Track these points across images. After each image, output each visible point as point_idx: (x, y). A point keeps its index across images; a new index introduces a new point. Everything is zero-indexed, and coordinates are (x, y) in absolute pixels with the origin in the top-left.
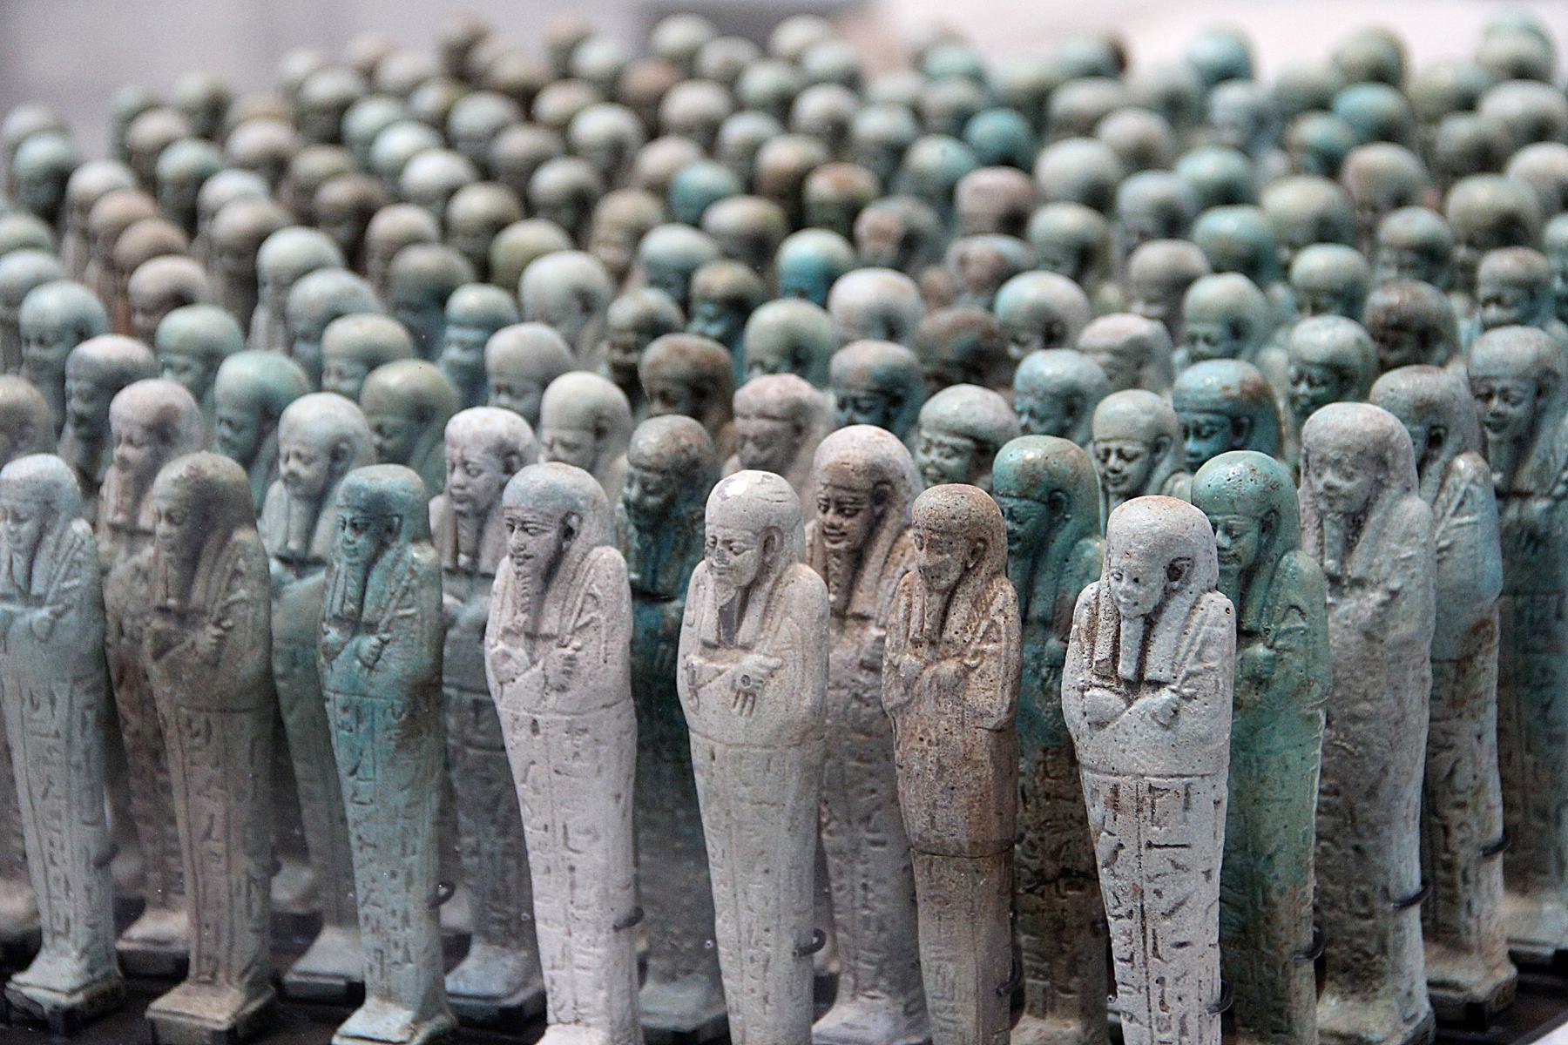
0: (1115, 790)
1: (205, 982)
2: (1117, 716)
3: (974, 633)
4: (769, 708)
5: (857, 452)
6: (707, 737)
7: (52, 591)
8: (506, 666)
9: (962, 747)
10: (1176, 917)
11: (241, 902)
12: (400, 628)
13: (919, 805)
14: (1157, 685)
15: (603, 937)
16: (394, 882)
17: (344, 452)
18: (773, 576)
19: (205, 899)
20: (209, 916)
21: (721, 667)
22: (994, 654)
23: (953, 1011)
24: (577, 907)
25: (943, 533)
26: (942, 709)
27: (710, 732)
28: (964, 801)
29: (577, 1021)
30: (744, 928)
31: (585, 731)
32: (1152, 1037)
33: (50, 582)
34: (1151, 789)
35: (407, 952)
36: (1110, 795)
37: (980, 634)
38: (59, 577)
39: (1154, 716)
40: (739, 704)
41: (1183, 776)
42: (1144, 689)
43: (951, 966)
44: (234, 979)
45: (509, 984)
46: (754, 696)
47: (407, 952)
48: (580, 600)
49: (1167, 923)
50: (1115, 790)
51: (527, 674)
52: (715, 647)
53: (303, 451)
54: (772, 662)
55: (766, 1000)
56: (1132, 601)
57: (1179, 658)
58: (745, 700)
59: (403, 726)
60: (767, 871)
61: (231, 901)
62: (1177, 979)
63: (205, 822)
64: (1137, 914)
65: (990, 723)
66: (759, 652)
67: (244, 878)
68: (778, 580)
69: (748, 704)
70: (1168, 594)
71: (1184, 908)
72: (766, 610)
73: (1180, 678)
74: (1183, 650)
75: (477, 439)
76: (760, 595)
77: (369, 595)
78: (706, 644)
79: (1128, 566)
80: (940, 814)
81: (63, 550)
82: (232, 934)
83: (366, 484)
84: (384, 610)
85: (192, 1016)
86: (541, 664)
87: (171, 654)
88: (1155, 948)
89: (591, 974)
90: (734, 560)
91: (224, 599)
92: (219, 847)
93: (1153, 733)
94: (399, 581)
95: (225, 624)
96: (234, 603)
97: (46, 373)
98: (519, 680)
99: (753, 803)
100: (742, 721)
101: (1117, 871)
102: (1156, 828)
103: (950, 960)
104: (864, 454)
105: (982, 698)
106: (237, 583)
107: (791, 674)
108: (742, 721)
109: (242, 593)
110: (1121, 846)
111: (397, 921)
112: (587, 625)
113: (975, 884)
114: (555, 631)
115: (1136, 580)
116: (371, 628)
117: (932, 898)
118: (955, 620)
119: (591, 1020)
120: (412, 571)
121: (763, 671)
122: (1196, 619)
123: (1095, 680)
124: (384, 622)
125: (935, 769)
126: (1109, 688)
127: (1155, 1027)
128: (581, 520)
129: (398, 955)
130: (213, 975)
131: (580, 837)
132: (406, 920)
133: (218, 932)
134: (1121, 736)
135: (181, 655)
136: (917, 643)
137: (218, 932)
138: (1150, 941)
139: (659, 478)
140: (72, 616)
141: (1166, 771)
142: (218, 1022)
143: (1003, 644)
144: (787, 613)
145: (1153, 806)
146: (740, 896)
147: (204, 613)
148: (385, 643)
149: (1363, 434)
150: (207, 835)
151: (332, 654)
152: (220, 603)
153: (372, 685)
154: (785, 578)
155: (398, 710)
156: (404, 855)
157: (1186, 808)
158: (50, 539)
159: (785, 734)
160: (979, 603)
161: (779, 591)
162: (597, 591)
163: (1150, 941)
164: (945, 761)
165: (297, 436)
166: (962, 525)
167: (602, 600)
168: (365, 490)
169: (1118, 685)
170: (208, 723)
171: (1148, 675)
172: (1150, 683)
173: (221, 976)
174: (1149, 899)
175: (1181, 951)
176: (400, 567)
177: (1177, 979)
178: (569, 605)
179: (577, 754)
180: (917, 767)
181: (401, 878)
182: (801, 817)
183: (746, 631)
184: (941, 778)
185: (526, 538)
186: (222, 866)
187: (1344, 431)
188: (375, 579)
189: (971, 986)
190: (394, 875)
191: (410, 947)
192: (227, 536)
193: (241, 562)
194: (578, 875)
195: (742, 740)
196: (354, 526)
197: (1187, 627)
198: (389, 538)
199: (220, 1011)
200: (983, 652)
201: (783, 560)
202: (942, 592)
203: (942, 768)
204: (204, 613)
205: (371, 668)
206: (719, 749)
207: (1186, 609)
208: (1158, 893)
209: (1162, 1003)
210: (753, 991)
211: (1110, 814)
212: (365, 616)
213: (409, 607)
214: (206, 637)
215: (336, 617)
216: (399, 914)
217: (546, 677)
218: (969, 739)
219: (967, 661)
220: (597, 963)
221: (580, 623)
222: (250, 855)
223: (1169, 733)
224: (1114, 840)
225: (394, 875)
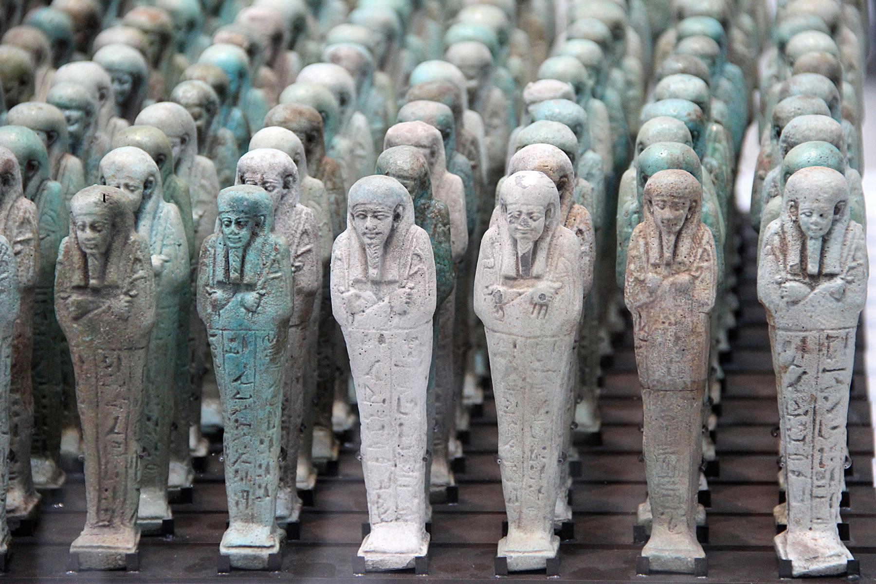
0: (804, 340)
1: (104, 526)
2: (806, 296)
3: (695, 256)
4: (557, 312)
5: (550, 159)
6: (510, 334)
8: (358, 303)
9: (691, 324)
10: (834, 412)
11: (131, 471)
12: (272, 286)
13: (660, 362)
14: (832, 276)
15: (418, 465)
16: (263, 446)
17: (151, 182)
18: (550, 233)
19: (106, 472)
20: (107, 483)
21: (521, 291)
22: (708, 268)
23: (674, 483)
24: (402, 449)
25: (680, 198)
26: (678, 303)
27: (514, 331)
28: (690, 357)
29: (397, 519)
30: (527, 450)
31: (416, 338)
32: (812, 483)
34: (828, 337)
35: (266, 490)
36: (800, 343)
37: (699, 257)
39: (832, 294)
40: (536, 312)
41: (845, 328)
42: (822, 279)
43: (673, 457)
44: (126, 522)
45: (287, 508)
46: (547, 306)
47: (266, 490)
48: (410, 258)
49: (830, 415)
50: (804, 340)
51: (375, 306)
52: (515, 279)
53: (131, 183)
54: (557, 285)
55: (539, 492)
56: (819, 228)
57: (843, 260)
58: (540, 310)
59: (273, 347)
60: (547, 412)
61: (127, 472)
62: (831, 448)
63: (111, 422)
64: (811, 413)
65: (707, 309)
66: (547, 280)
67: (135, 456)
68: (553, 236)
69: (543, 312)
70: (835, 222)
71: (839, 406)
72: (548, 254)
73: (845, 271)
74: (845, 255)
75: (272, 167)
76: (544, 245)
77: (248, 267)
78: (508, 278)
79: (818, 207)
80: (674, 367)
82: (125, 494)
83: (246, 196)
84: (260, 275)
85: (109, 548)
86: (387, 299)
87: (90, 315)
88: (820, 431)
89: (410, 489)
90: (533, 224)
91: (130, 277)
92: (120, 438)
93: (831, 305)
95: (132, 293)
96: (136, 280)
98: (367, 311)
99: (543, 371)
100: (538, 322)
101: (799, 388)
102: (829, 360)
103: (673, 453)
104: (555, 159)
105: (703, 295)
106: (138, 266)
107: (568, 290)
108: (538, 322)
109: (141, 273)
110: (805, 373)
111: (262, 471)
112: (416, 273)
113: (692, 406)
114: (397, 279)
115: (821, 215)
116: (250, 287)
117: (662, 417)
118: (684, 249)
119: (409, 518)
120: (276, 249)
121: (552, 291)
122: (850, 236)
123: (789, 277)
124: (260, 282)
125: (673, 339)
126: (798, 281)
127: (814, 478)
128: (404, 209)
129: (261, 493)
130: (110, 521)
131: (408, 405)
132: (267, 471)
133: (115, 493)
134: (809, 308)
135: (99, 315)
136: (656, 266)
137: (115, 493)
138: (817, 427)
139: (413, 183)
141: (838, 326)
142: (129, 549)
143: (712, 261)
144: (561, 255)
145: (829, 347)
146: (527, 429)
147: (118, 287)
148: (262, 295)
149: (832, 132)
150: (111, 431)
151: (217, 306)
152: (128, 280)
154: (557, 234)
155: (272, 337)
156: (268, 428)
157: (845, 347)
159: (565, 328)
160: (696, 239)
161: (554, 242)
162: (420, 252)
163: (817, 427)
164: (680, 334)
165: (126, 174)
166: (690, 192)
167: (423, 257)
168: (246, 200)
169: (804, 278)
170: (119, 359)
171: (826, 270)
172: (826, 275)
173: (117, 521)
174: (820, 402)
175: (835, 431)
176: (267, 248)
177: (831, 448)
178: (403, 262)
179: (410, 353)
180: (660, 340)
181: (266, 444)
183: (538, 267)
184: (677, 345)
185: (376, 221)
186: (121, 449)
187: (821, 131)
188: (251, 256)
189: (687, 468)
190: (262, 442)
191: (269, 487)
192: (127, 238)
194: (405, 428)
195: (538, 333)
196: (238, 223)
197: (845, 241)
198: (257, 230)
199: (128, 542)
200: (701, 267)
201: (555, 223)
202: (674, 234)
203: (678, 338)
204: (118, 287)
205: (254, 312)
206: (520, 341)
207: (844, 231)
208: (826, 398)
209: (821, 463)
210: (530, 487)
211: (800, 354)
212: (247, 280)
213: (276, 272)
214: (121, 302)
215: (219, 282)
216: (264, 466)
217: (392, 307)
218: (695, 319)
219: (693, 273)
220: (414, 482)
221: (412, 272)
222: (138, 440)
223: (840, 304)
224: (801, 370)
225: (262, 442)
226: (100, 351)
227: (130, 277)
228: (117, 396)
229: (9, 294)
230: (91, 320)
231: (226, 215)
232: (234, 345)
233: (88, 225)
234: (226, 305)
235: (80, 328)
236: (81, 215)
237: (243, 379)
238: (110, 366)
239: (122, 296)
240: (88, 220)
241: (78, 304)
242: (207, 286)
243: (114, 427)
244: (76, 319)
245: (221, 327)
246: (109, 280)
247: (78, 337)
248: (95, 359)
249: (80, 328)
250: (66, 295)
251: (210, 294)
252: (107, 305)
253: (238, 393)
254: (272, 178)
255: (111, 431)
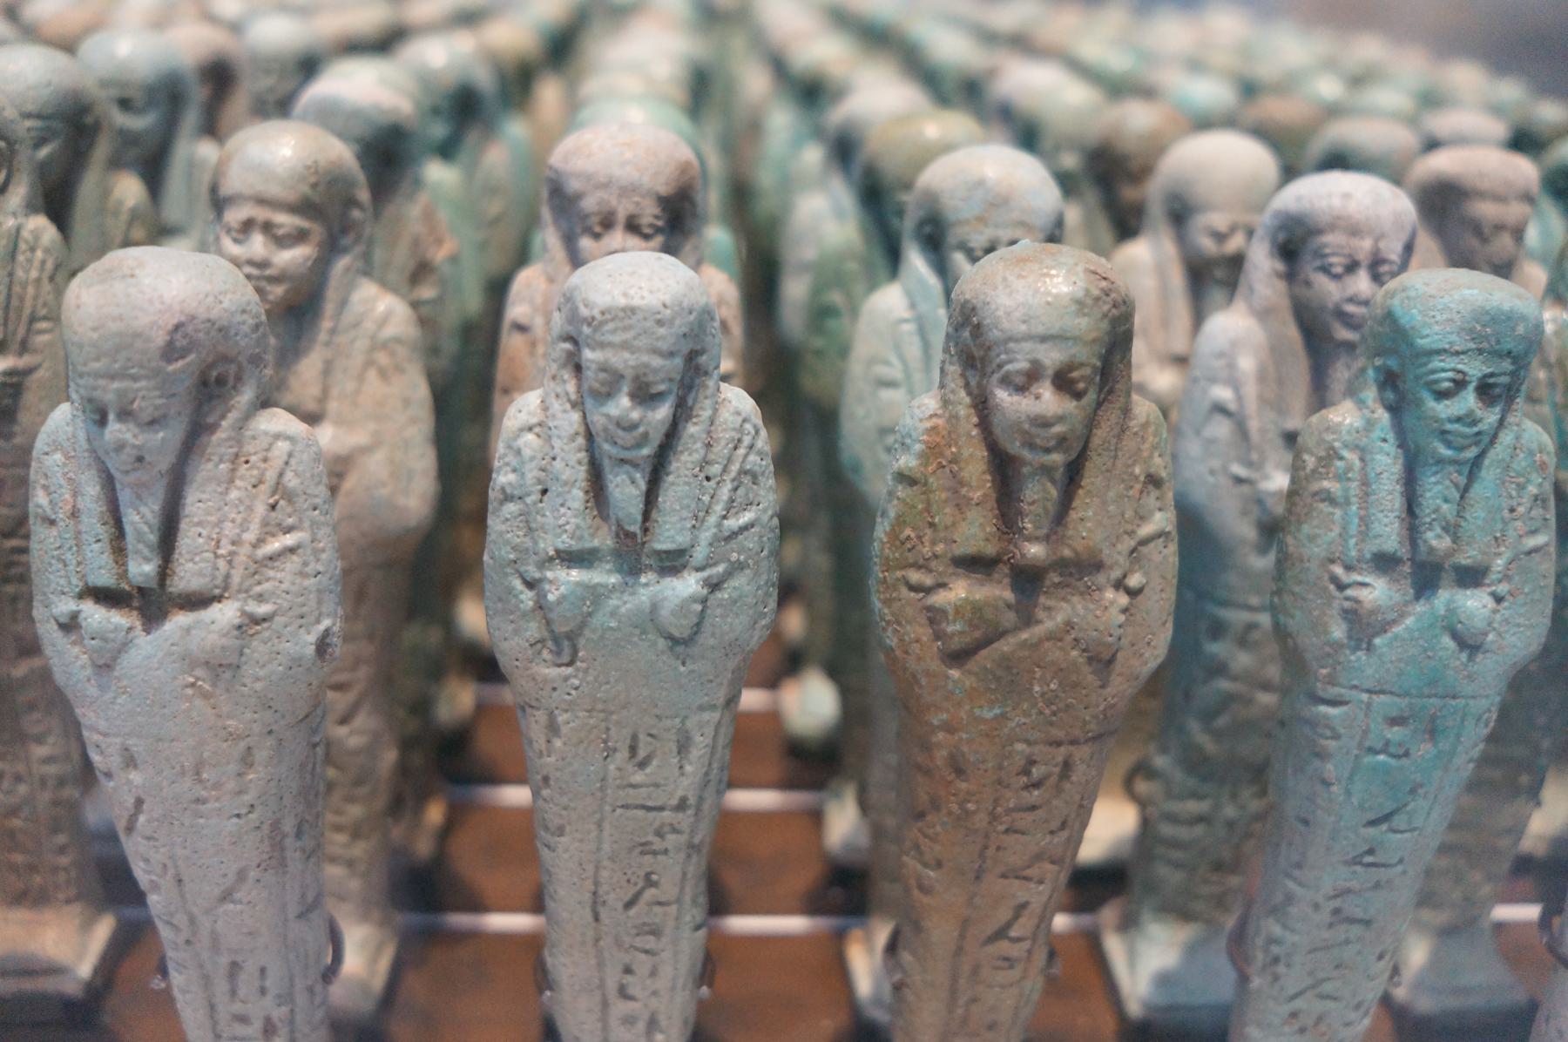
7: (706, 536)
33: (700, 515)
38: (719, 509)
63: (1004, 914)
81: (721, 450)
87: (1005, 646)
91: (1131, 533)
94: (1521, 487)
96: (1144, 542)
97: (133, 153)
116: (1471, 577)
124: (1499, 563)
135: (1035, 646)
140: (740, 582)
150: (1001, 934)
153: (1471, 678)
158: (692, 429)
182: (287, 801)
193: (1157, 460)
196: (1485, 390)
226: (1020, 747)
227: (1131, 533)
228: (1038, 857)
229: (757, 574)
230: (1006, 663)
231: (1451, 362)
232: (1395, 733)
233: (1050, 372)
234: (1394, 622)
235: (970, 682)
236: (1028, 337)
237: (1399, 821)
238: (1036, 785)
239: (1110, 594)
240: (1052, 357)
241: (974, 612)
242: (1332, 561)
243: (1009, 925)
244: (958, 657)
245: (1368, 684)
246: (1079, 545)
247: (959, 704)
248: (1000, 767)
249: (970, 682)
250: (928, 581)
251: (1342, 587)
252: (1060, 618)
253: (1371, 852)
254: (650, 213)
255: (1001, 934)
